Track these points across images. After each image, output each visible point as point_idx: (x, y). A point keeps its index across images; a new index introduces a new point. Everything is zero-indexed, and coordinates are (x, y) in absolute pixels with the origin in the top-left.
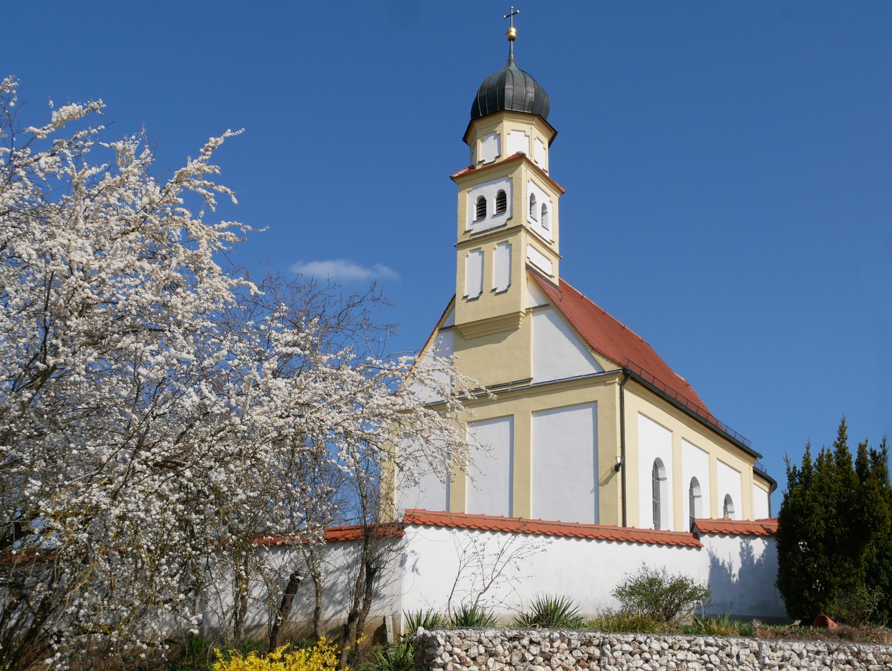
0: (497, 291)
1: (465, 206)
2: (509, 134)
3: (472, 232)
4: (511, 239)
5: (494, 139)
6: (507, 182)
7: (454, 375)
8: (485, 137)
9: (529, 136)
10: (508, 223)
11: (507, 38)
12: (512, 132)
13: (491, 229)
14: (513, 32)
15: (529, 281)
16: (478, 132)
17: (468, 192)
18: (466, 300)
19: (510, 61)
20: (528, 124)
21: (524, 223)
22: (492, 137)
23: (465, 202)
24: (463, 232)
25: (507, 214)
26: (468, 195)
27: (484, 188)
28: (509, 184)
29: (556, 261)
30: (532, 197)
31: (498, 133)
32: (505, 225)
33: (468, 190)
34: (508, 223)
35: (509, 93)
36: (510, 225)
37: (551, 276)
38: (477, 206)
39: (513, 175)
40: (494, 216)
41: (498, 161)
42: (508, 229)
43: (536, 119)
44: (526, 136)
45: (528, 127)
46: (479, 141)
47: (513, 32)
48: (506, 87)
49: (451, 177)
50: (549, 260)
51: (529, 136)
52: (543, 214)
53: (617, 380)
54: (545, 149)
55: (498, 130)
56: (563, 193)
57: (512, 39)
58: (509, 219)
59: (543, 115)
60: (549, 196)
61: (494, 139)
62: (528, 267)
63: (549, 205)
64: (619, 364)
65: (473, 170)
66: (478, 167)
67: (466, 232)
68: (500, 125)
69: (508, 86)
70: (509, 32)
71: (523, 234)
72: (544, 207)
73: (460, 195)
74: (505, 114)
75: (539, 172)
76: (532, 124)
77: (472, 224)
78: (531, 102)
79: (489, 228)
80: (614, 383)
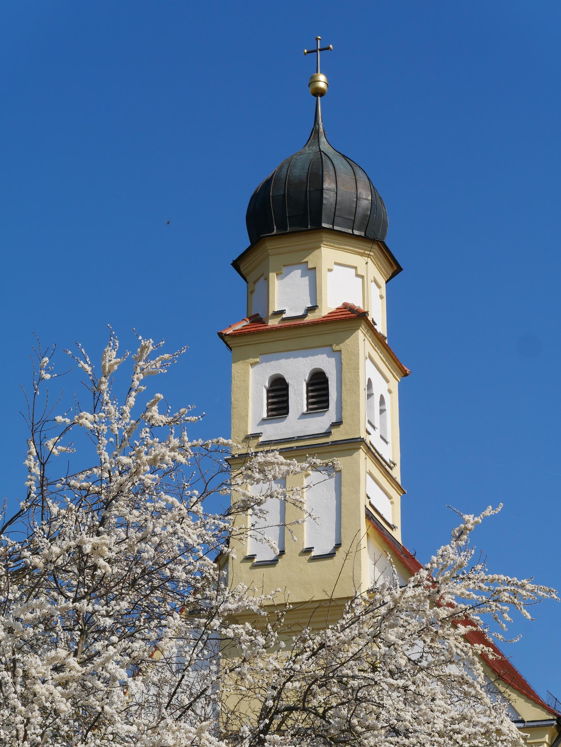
0: (313, 554)
1: (247, 389)
2: (330, 270)
3: (261, 439)
4: (340, 462)
5: (303, 276)
6: (329, 356)
7: (24, 601)
8: (284, 270)
9: (362, 277)
10: (333, 431)
11: (310, 90)
12: (336, 268)
13: (300, 439)
14: (322, 85)
15: (372, 540)
16: (271, 258)
17: (253, 365)
18: (249, 564)
19: (315, 132)
20: (362, 255)
21: (363, 435)
22: (297, 273)
23: (246, 381)
24: (242, 437)
25: (330, 416)
26: (251, 370)
27: (283, 361)
28: (333, 361)
29: (397, 497)
30: (370, 384)
31: (310, 266)
32: (328, 434)
33: (252, 360)
34: (333, 431)
35: (329, 197)
36: (337, 435)
37: (392, 527)
38: (268, 391)
39: (342, 346)
40: (304, 415)
41: (311, 317)
42: (335, 443)
43: (375, 247)
44: (357, 275)
45: (363, 260)
46: (272, 276)
47: (322, 81)
48: (326, 186)
49: (221, 335)
50: (390, 497)
51: (362, 277)
52: (382, 411)
53: (547, 738)
54: (381, 297)
55: (311, 260)
56: (406, 375)
57: (319, 93)
58: (337, 424)
59: (379, 237)
60: (388, 381)
61: (303, 276)
62: (369, 516)
63: (387, 397)
64: (550, 711)
65: (262, 327)
66: (273, 323)
67: (248, 438)
68: (316, 252)
69: (328, 185)
70: (313, 81)
71: (362, 454)
72: (382, 401)
73: (237, 368)
74: (325, 236)
75: (378, 338)
76: (368, 256)
77: (259, 425)
78: (365, 216)
79: (295, 435)
80: (542, 743)
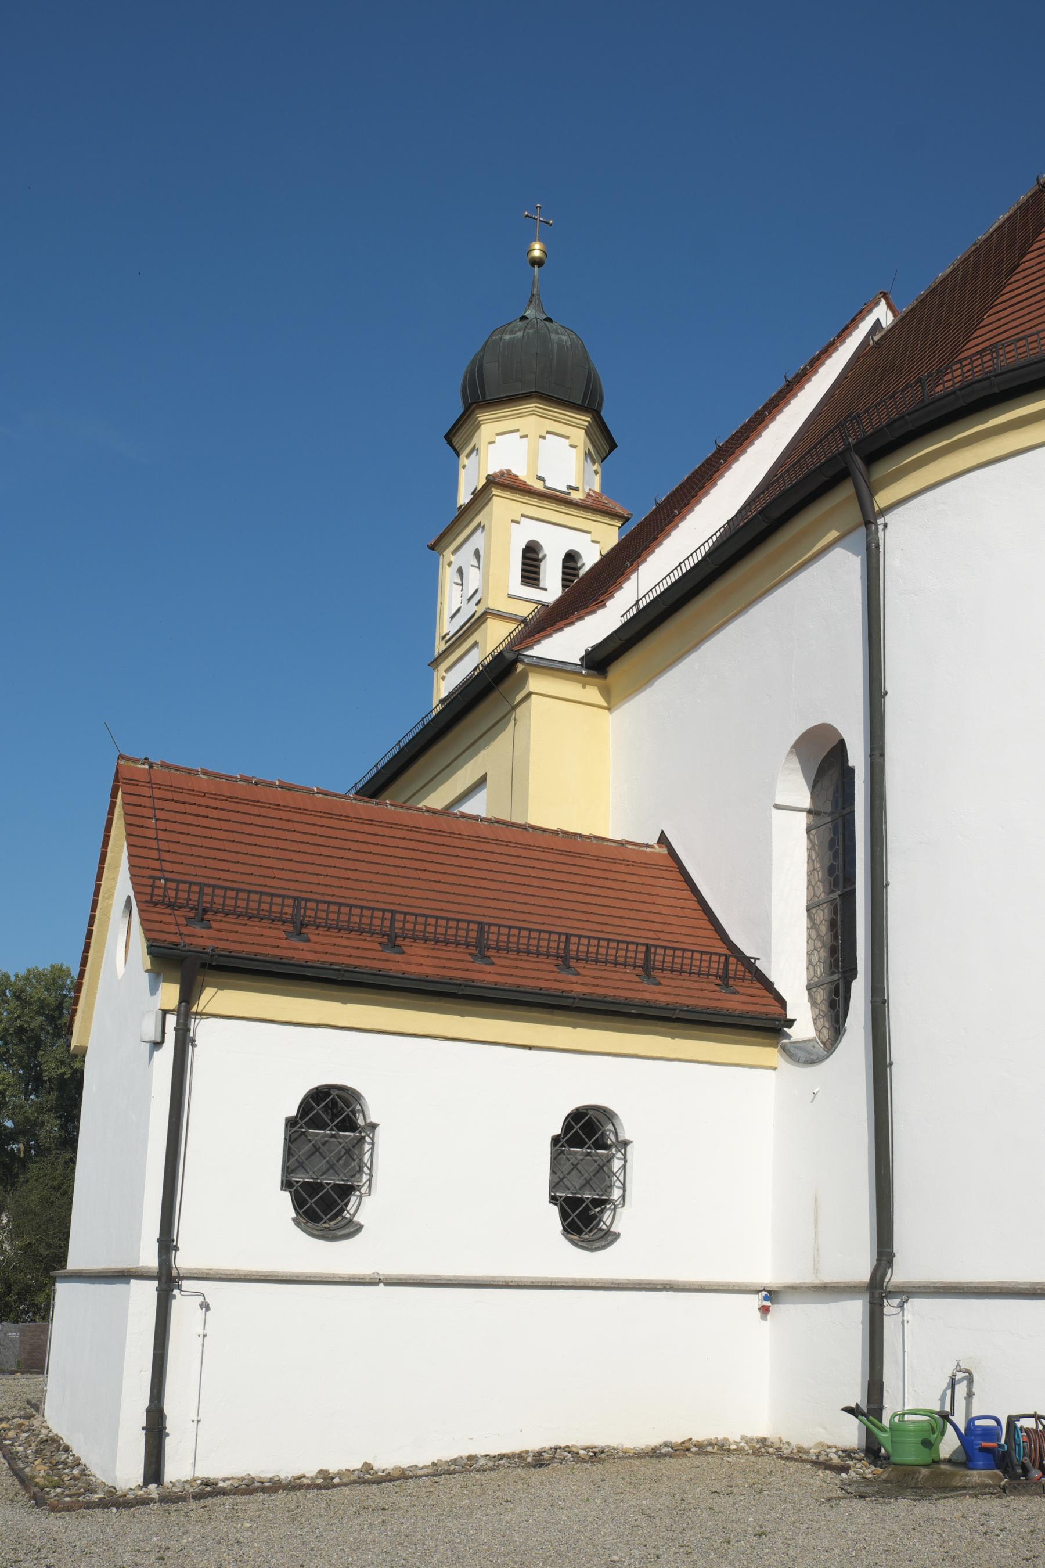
14: (537, 253)
43: (532, 406)
57: (537, 263)
